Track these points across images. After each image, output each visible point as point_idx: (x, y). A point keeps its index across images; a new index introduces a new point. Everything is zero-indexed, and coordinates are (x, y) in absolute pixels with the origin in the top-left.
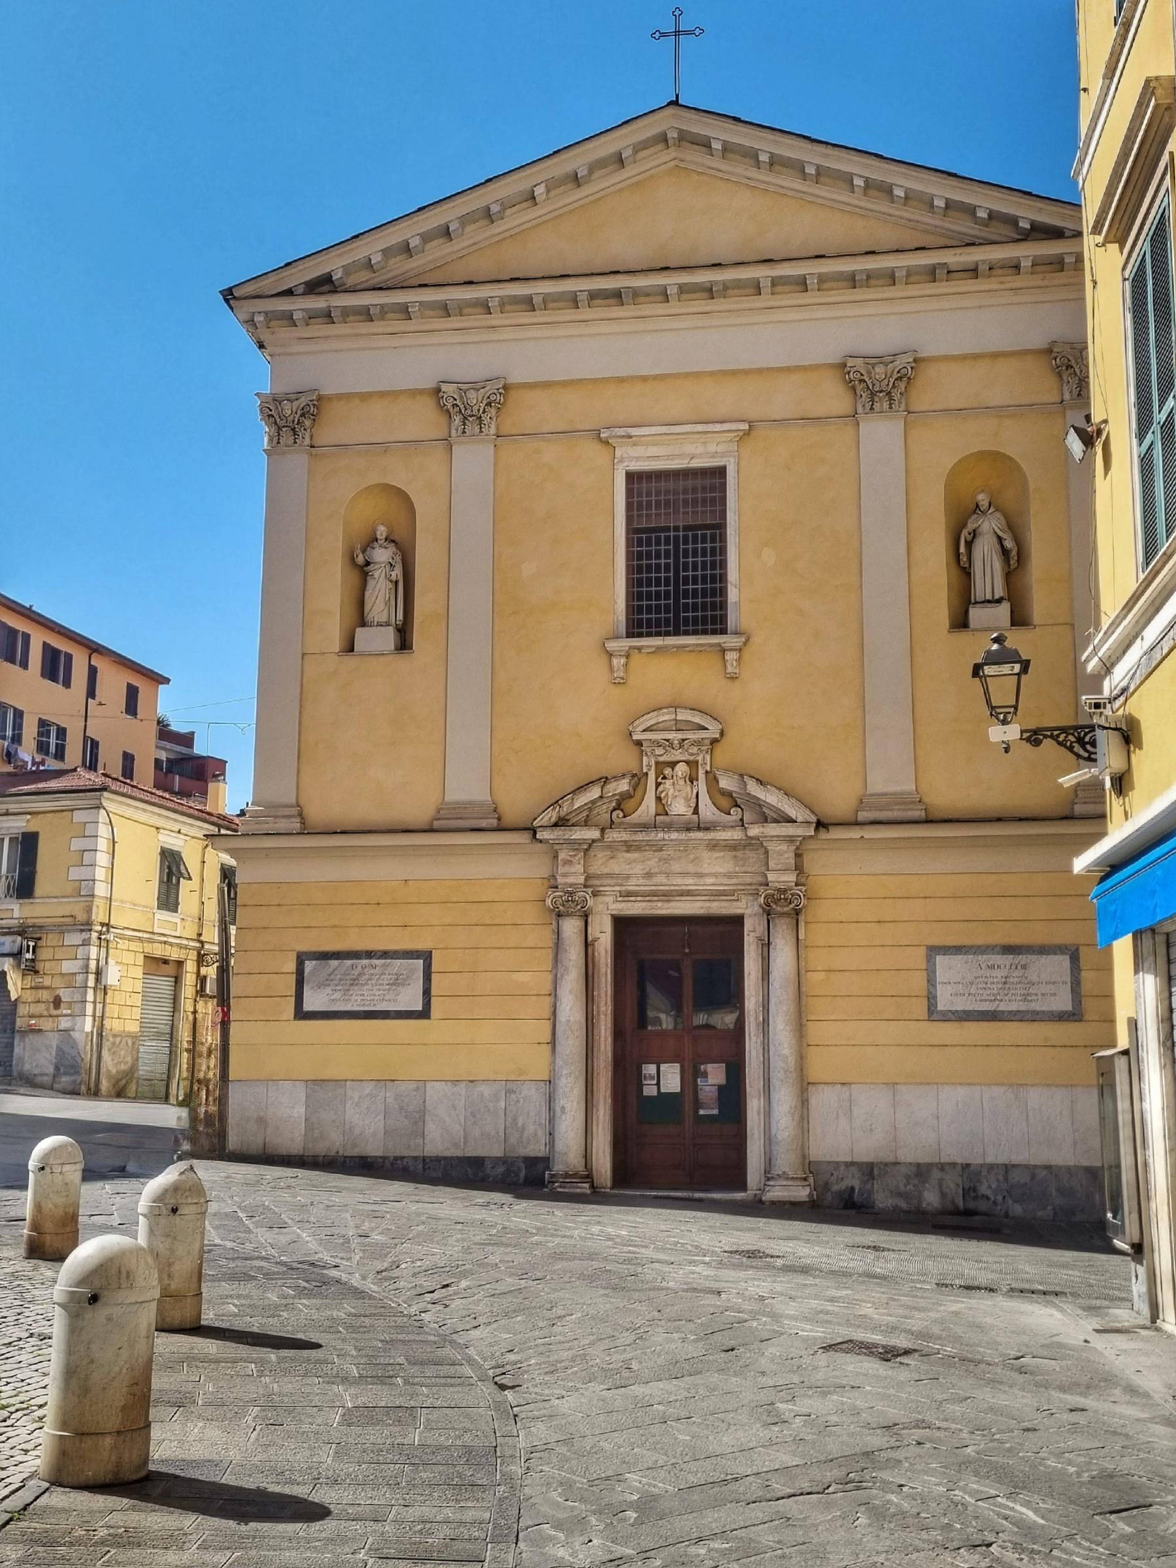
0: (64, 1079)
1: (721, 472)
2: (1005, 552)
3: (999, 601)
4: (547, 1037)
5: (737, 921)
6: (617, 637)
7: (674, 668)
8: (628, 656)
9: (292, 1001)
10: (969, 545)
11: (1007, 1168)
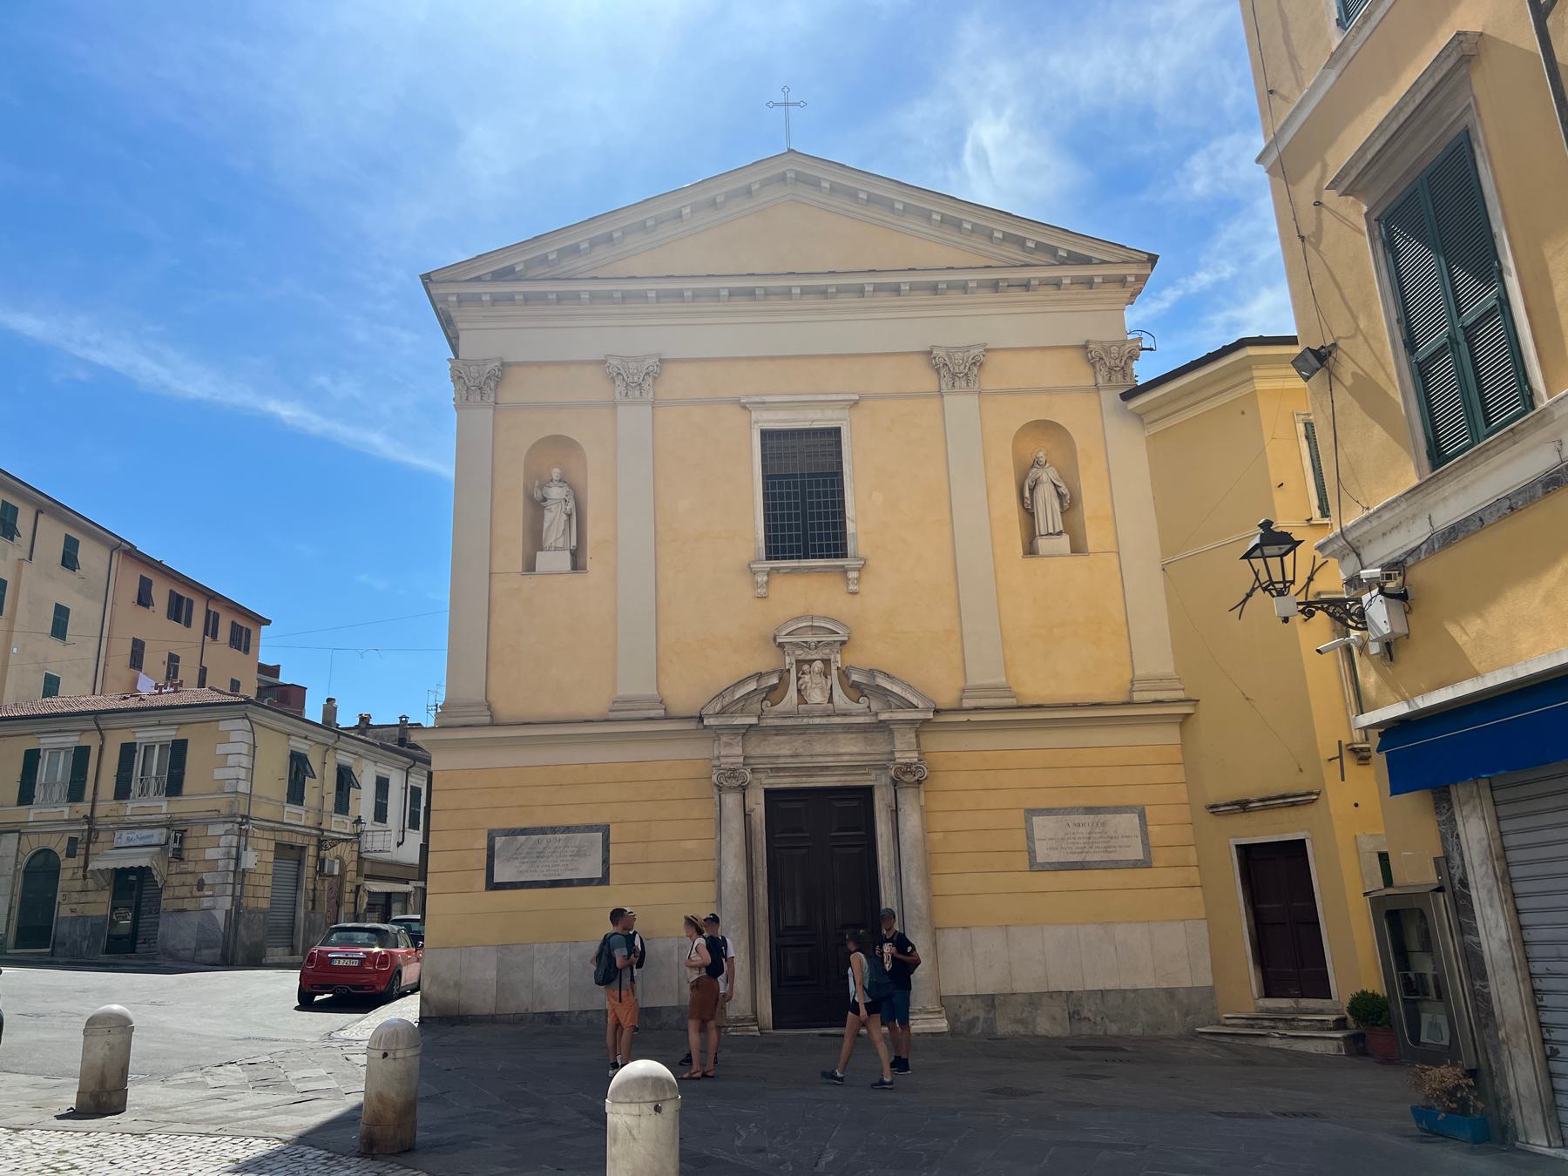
0: (205, 952)
1: (838, 430)
2: (1060, 496)
3: (1060, 533)
4: (713, 897)
5: (868, 792)
6: (759, 561)
7: (806, 591)
8: (768, 574)
9: (484, 873)
10: (1032, 490)
11: (1103, 993)
